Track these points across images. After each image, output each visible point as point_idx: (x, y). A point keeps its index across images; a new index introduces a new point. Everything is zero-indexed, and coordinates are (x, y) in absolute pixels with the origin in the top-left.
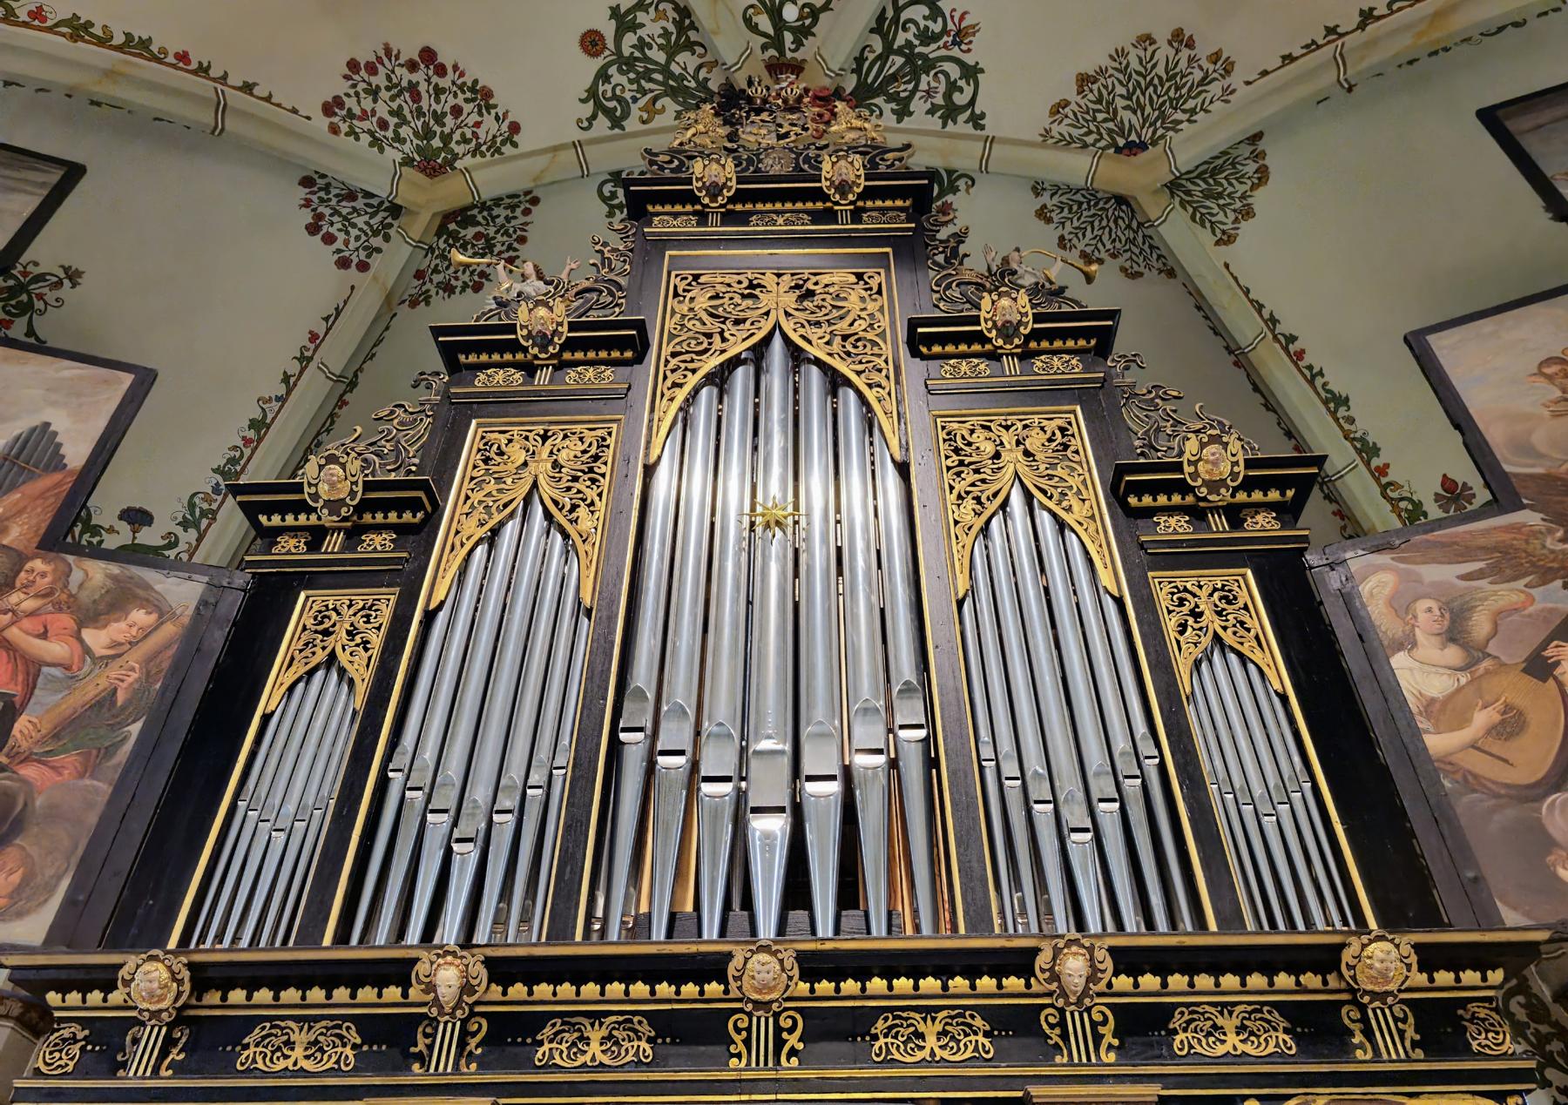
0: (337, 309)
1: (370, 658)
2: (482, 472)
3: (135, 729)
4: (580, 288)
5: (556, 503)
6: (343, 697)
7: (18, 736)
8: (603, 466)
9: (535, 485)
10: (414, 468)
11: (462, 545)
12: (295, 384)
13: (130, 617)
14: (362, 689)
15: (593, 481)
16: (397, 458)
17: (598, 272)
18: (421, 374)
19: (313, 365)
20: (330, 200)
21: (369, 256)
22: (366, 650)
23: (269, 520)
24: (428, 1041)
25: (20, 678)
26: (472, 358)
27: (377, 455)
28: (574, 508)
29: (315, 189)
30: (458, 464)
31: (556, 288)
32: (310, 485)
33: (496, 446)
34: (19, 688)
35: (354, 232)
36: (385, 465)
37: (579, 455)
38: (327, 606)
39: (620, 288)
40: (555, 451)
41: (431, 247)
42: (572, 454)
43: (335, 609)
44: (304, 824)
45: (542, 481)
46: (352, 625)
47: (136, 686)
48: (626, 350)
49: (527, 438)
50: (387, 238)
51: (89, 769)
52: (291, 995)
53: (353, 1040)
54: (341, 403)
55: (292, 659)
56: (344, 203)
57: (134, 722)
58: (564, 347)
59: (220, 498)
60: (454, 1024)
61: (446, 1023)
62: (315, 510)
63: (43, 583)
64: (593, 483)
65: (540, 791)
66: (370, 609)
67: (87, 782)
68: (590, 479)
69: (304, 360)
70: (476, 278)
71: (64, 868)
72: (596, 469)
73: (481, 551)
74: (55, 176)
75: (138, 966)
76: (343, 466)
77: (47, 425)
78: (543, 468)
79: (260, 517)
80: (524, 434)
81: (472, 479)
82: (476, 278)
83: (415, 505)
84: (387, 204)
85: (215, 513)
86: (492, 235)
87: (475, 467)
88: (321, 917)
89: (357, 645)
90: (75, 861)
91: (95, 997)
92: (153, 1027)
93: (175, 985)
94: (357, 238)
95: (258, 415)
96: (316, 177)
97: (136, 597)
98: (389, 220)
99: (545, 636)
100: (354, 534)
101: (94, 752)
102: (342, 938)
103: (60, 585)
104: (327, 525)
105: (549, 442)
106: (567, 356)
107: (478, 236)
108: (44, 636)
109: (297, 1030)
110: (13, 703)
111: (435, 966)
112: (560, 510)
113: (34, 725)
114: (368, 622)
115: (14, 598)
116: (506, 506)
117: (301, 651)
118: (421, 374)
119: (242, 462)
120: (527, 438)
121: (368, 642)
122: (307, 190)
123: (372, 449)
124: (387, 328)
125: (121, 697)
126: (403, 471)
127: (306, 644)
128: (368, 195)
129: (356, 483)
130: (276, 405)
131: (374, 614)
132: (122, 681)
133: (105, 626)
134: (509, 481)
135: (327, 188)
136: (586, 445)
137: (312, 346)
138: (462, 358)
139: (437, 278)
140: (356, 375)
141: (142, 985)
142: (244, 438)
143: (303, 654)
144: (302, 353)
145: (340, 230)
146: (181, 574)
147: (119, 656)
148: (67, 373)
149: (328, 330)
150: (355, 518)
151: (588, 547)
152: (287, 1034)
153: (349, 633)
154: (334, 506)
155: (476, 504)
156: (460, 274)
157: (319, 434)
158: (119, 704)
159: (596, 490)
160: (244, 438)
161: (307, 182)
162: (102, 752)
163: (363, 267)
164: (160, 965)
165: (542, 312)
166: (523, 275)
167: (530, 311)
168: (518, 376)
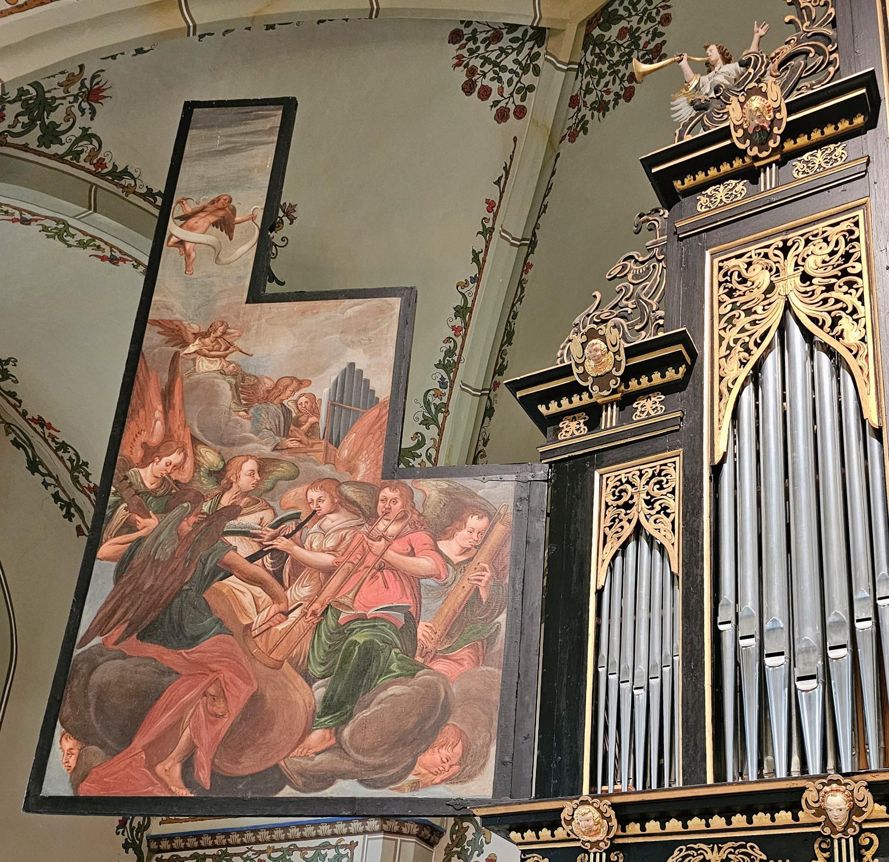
0: (505, 168)
1: (673, 523)
2: (729, 307)
3: (502, 618)
4: (782, 57)
5: (815, 320)
6: (658, 563)
7: (423, 639)
8: (857, 264)
9: (788, 306)
10: (661, 322)
11: (730, 390)
12: (484, 261)
13: (467, 524)
14: (674, 553)
15: (850, 284)
16: (642, 315)
17: (798, 29)
18: (641, 216)
19: (496, 235)
20: (478, 48)
21: (523, 99)
22: (668, 515)
23: (548, 408)
24: (827, 855)
25: (408, 591)
26: (689, 182)
27: (623, 317)
28: (836, 321)
29: (464, 42)
30: (703, 302)
31: (755, 68)
32: (577, 365)
33: (736, 274)
34: (410, 600)
35: (505, 76)
36: (633, 325)
37: (827, 258)
38: (620, 480)
39: (828, 40)
40: (800, 262)
41: (580, 64)
42: (819, 260)
43: (628, 482)
44: (658, 680)
45: (795, 301)
46: (648, 494)
47: (491, 583)
48: (855, 116)
49: (766, 256)
50: (537, 72)
51: (481, 658)
52: (696, 823)
53: (759, 857)
54: (527, 267)
55: (605, 536)
56: (491, 47)
57: (500, 613)
58: (784, 137)
59: (447, 391)
60: (847, 840)
61: (840, 840)
62: (586, 389)
63: (397, 508)
64: (850, 287)
65: (869, 624)
66: (659, 475)
67: (483, 668)
68: (845, 283)
69: (487, 232)
70: (626, 84)
71: (488, 739)
72: (850, 270)
73: (748, 395)
74: (276, 118)
75: (574, 810)
76: (603, 338)
77: (352, 365)
78: (790, 285)
79: (539, 407)
80: (763, 251)
81: (721, 317)
82: (626, 84)
83: (675, 360)
84: (531, 31)
85: (446, 405)
86: (635, 26)
87: (720, 303)
88: (699, 758)
89: (658, 513)
90: (494, 731)
91: (545, 833)
92: (595, 854)
93: (605, 821)
94: (510, 82)
95: (459, 302)
96: (462, 27)
97: (466, 506)
98: (536, 49)
99: (835, 468)
100: (626, 402)
101: (480, 643)
102: (720, 776)
103: (409, 508)
104: (599, 401)
105: (791, 253)
106: (789, 145)
107: (622, 33)
108: (412, 553)
109: (709, 851)
110: (410, 613)
111: (822, 793)
112: (822, 327)
113: (430, 628)
114: (661, 488)
115: (381, 526)
116: (763, 338)
117: (610, 527)
118: (641, 216)
119: (457, 352)
120: (766, 256)
121: (667, 508)
122: (457, 46)
123: (616, 313)
124: (553, 173)
125: (484, 594)
126: (652, 328)
127: (613, 520)
128: (512, 28)
129: (617, 353)
130: (472, 287)
131: (664, 479)
132: (480, 581)
133: (452, 537)
134: (759, 309)
135: (473, 38)
136: (832, 244)
137: (491, 215)
138: (678, 184)
139: (591, 98)
140: (534, 234)
141: (582, 823)
142: (453, 328)
143: (613, 530)
144: (484, 226)
145: (492, 79)
146: (494, 477)
147: (471, 560)
148: (350, 312)
149: (502, 193)
150: (622, 388)
151: (861, 361)
152: (701, 854)
153: (648, 502)
154: (602, 380)
155: (732, 344)
156: (610, 86)
157: (513, 305)
158: (484, 601)
159: (855, 295)
160: (453, 328)
161: (455, 37)
162: (485, 641)
163: (520, 112)
164: (591, 807)
165: (756, 102)
166: (707, 64)
167: (742, 104)
168: (740, 187)
